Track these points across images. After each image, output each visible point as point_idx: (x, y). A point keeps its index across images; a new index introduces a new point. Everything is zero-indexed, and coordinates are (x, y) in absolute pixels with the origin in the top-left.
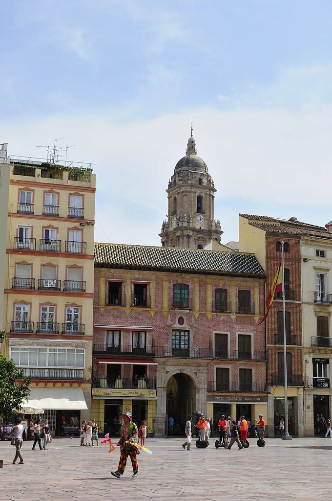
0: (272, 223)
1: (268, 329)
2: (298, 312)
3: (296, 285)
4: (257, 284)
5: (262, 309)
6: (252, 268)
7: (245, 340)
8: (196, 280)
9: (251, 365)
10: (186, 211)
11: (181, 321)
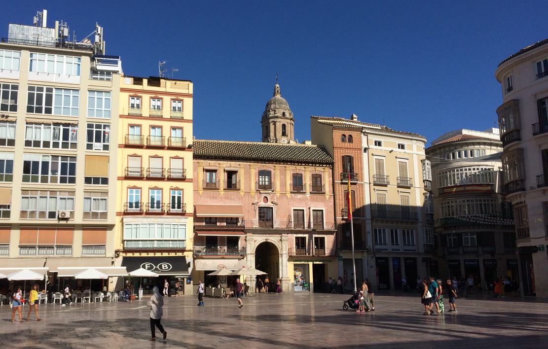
3: (358, 168)
11: (266, 199)
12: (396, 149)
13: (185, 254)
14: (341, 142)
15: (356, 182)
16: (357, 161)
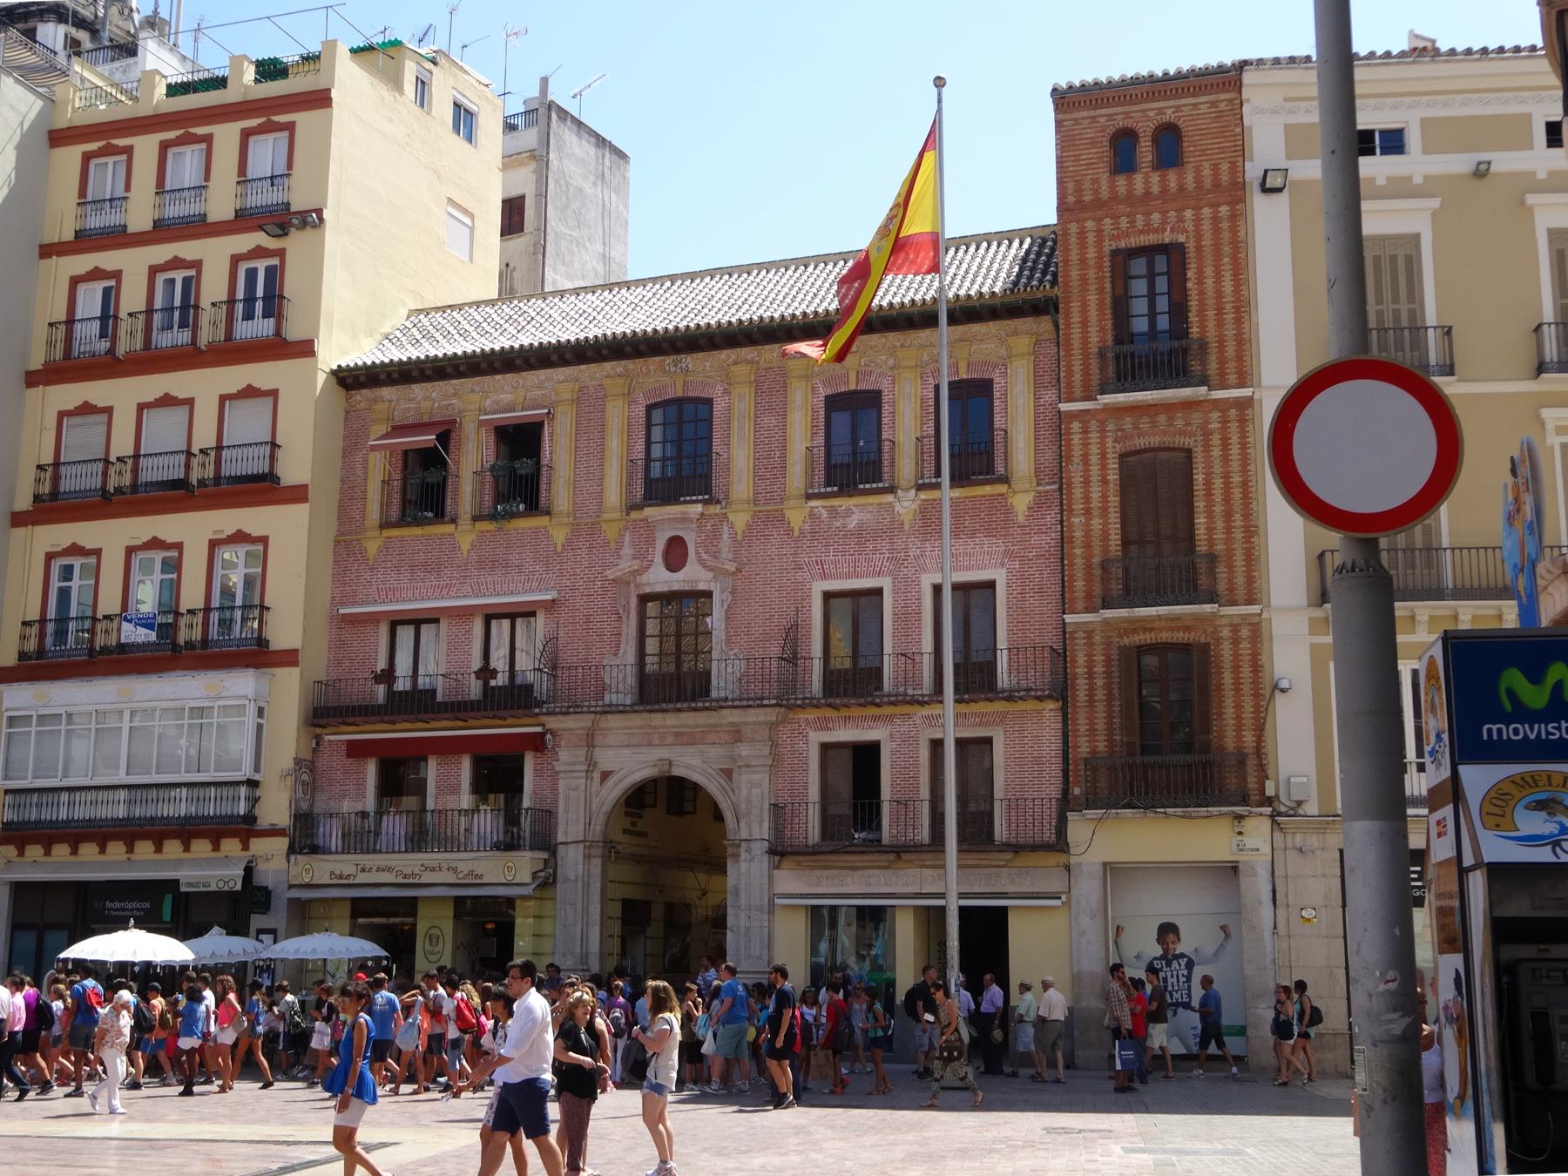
2: (1235, 439)
4: (1023, 343)
8: (741, 370)
9: (985, 720)
11: (675, 554)
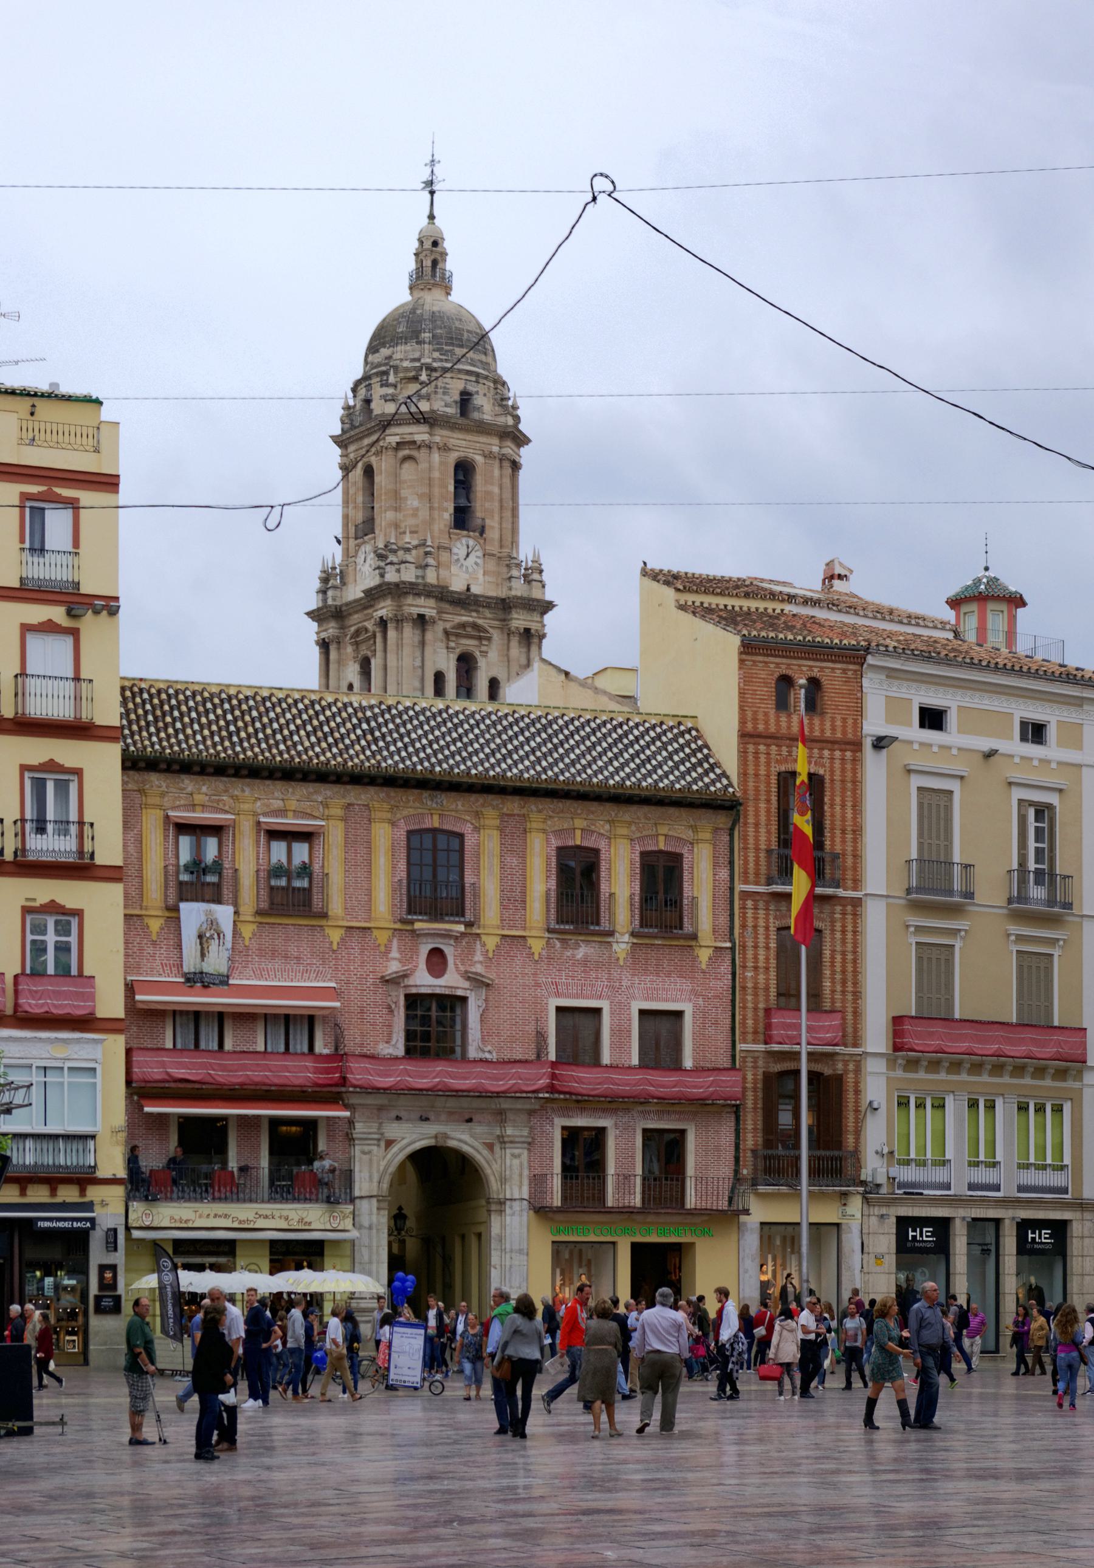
0: (761, 605)
1: (744, 988)
2: (850, 928)
3: (843, 832)
5: (723, 920)
6: (688, 772)
7: (661, 1029)
10: (411, 521)
11: (437, 961)
12: (1014, 746)
13: (94, 1193)
14: (772, 712)
15: (829, 891)
16: (838, 800)
